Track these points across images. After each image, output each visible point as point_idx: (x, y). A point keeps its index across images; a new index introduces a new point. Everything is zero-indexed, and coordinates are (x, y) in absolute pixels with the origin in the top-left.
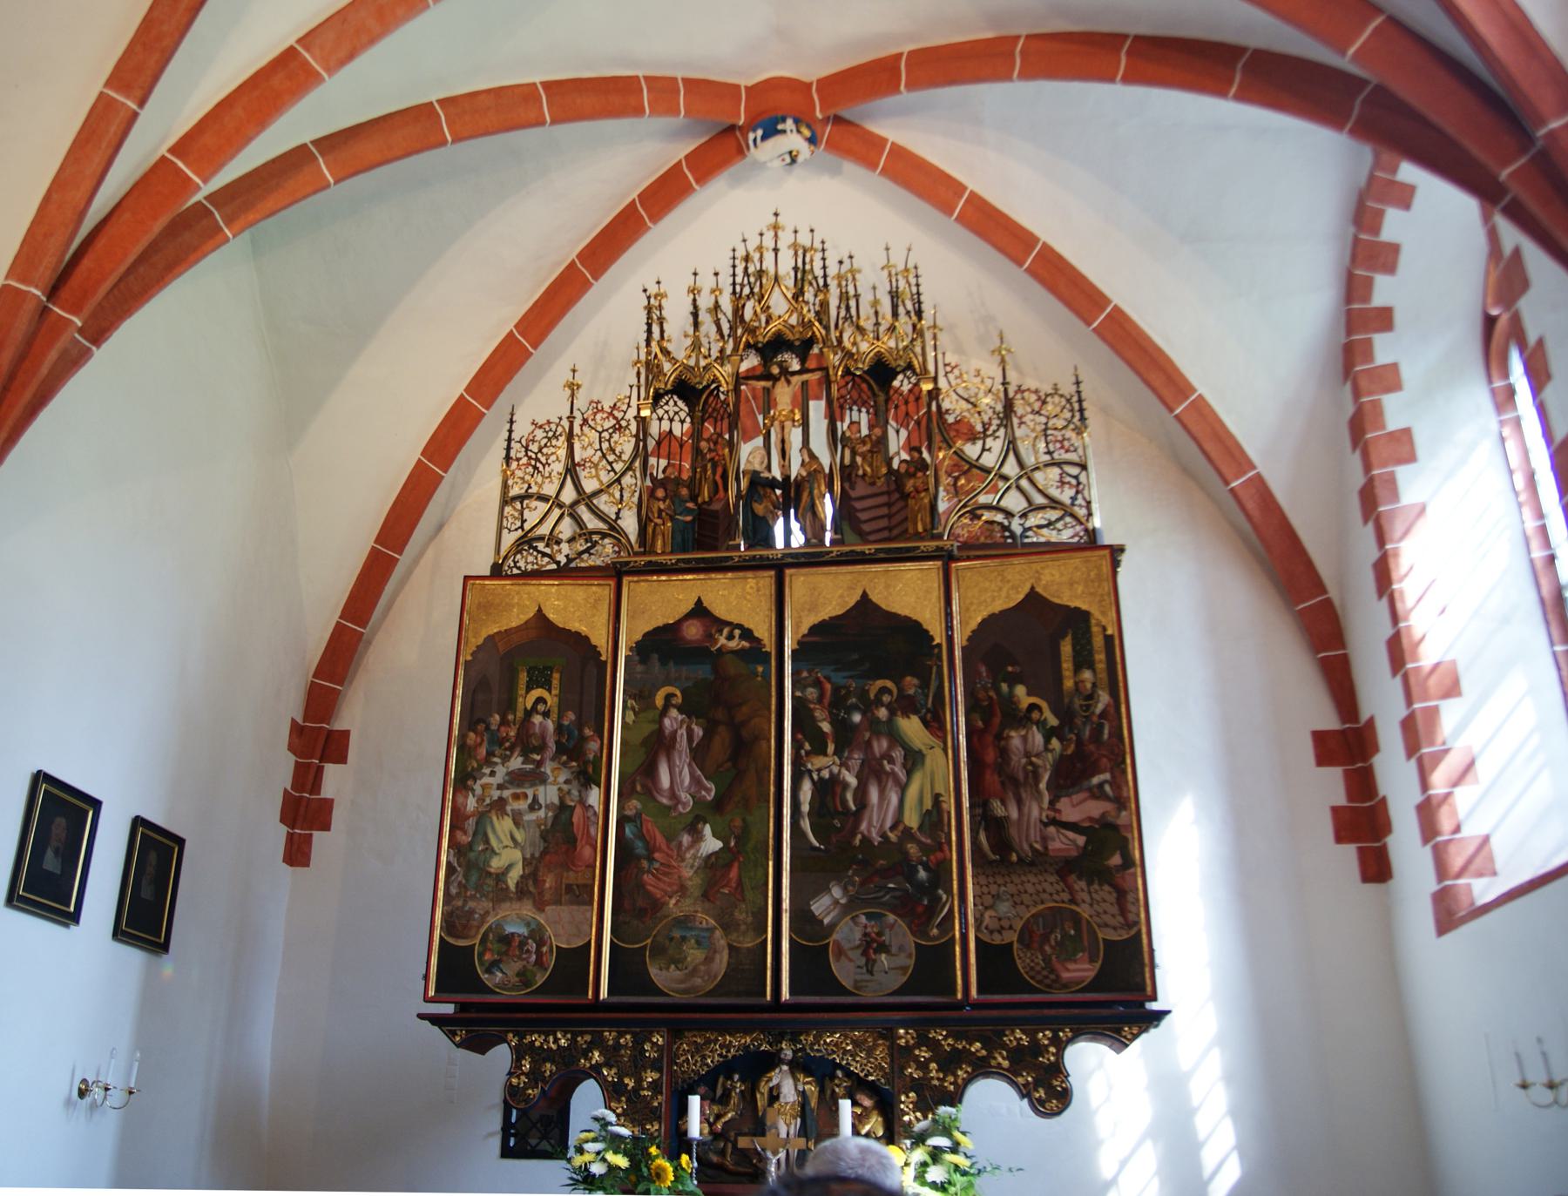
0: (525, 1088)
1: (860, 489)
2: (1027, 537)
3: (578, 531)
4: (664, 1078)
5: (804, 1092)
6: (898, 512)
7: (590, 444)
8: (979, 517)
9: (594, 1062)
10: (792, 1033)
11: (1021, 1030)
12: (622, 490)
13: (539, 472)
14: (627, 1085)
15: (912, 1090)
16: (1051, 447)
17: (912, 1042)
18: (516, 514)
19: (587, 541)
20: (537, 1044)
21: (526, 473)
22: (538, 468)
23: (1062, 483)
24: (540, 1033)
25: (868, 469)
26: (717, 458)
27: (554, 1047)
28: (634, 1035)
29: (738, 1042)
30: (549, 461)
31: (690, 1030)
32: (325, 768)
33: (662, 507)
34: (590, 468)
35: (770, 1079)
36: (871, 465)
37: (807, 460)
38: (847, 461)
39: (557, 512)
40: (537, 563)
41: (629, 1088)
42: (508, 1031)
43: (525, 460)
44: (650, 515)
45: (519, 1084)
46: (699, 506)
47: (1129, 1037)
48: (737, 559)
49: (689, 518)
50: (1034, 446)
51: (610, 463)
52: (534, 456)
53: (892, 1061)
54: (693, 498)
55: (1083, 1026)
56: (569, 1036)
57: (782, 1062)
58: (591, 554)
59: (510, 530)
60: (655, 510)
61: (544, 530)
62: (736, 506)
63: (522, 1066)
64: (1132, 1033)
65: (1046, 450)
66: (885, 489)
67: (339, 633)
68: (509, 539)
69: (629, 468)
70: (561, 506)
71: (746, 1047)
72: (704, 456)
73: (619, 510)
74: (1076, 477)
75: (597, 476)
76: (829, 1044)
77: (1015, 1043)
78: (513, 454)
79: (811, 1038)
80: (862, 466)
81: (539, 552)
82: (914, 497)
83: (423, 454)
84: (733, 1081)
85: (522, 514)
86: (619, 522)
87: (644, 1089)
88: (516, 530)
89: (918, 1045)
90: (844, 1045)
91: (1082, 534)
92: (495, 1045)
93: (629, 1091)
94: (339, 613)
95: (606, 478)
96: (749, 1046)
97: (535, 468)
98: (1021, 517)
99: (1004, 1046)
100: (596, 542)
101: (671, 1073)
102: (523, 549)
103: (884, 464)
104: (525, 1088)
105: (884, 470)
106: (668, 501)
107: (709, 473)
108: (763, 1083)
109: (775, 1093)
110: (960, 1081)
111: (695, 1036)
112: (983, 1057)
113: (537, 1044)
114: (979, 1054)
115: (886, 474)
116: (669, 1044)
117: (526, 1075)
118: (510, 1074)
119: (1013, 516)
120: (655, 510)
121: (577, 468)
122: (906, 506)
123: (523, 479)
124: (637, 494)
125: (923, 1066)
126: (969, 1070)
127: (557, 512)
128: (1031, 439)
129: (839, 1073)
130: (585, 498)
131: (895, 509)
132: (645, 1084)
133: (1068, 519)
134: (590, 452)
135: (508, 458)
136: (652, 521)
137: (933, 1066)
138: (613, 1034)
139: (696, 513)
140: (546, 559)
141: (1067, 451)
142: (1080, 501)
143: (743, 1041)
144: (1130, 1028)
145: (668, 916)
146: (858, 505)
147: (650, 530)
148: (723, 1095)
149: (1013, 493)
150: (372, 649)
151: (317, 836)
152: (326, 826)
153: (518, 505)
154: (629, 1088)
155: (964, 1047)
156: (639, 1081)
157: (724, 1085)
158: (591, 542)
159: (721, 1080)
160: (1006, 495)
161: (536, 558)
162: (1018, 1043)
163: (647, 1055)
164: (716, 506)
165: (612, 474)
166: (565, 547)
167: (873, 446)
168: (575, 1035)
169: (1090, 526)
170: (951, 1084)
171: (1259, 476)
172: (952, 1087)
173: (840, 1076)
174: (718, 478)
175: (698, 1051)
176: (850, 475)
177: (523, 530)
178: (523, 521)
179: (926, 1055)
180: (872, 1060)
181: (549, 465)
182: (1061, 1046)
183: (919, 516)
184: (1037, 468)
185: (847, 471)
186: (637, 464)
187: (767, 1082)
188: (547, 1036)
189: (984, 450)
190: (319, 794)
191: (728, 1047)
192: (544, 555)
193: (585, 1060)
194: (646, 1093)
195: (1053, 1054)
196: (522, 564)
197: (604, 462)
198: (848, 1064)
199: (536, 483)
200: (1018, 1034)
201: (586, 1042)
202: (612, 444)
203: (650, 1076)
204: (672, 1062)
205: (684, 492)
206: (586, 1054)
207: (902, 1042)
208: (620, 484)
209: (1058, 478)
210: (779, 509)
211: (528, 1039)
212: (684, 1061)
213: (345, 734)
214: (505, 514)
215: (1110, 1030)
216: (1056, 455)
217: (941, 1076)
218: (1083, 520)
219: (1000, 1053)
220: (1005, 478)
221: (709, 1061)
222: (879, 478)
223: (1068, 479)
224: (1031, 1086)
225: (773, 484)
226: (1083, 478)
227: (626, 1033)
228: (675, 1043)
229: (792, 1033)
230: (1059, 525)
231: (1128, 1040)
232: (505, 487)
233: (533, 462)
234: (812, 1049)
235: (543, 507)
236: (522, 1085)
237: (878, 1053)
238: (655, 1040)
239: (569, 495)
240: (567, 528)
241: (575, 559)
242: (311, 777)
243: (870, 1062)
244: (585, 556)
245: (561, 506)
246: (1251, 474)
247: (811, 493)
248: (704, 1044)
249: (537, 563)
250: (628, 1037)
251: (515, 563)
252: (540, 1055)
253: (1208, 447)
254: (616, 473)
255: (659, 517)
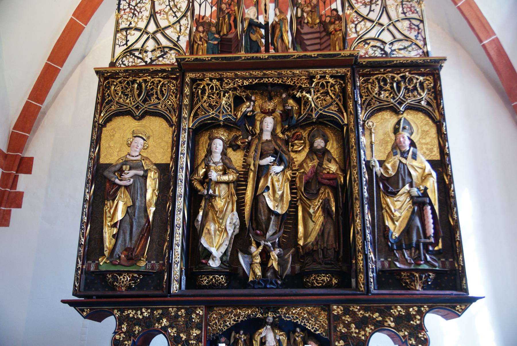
0: (124, 341)
1: (306, 29)
2: (393, 54)
3: (157, 46)
4: (203, 333)
5: (279, 340)
6: (325, 42)
7: (164, 3)
8: (369, 44)
9: (163, 325)
10: (274, 308)
11: (400, 306)
12: (180, 26)
13: (136, 16)
14: (182, 337)
15: (341, 339)
16: (405, 10)
17: (340, 312)
18: (123, 37)
19: (161, 51)
20: (131, 315)
21: (129, 17)
22: (135, 14)
23: (410, 28)
24: (132, 309)
25: (310, 19)
26: (231, 12)
27: (141, 317)
28: (186, 309)
29: (244, 313)
30: (141, 11)
31: (217, 307)
32: (19, 177)
33: (202, 36)
34: (164, 14)
35: (261, 333)
36: (311, 18)
37: (278, 13)
38: (299, 15)
39: (145, 37)
40: (134, 62)
41: (183, 339)
42: (114, 309)
43: (128, 10)
44: (195, 39)
45: (120, 338)
46: (221, 37)
47: (460, 311)
48: (243, 58)
49: (216, 42)
50: (396, 9)
51: (174, 13)
52: (133, 8)
53: (329, 322)
54: (218, 33)
55: (435, 304)
56: (149, 311)
57: (267, 323)
58: (164, 58)
59: (120, 46)
60: (198, 37)
61: (138, 45)
62: (241, 36)
63: (122, 328)
64: (461, 309)
65: (402, 12)
66: (318, 30)
67: (27, 106)
68: (119, 50)
69: (184, 15)
70: (147, 33)
71: (249, 315)
72: (223, 12)
73: (179, 36)
74: (418, 26)
75: (167, 19)
76: (294, 314)
77: (397, 313)
78: (121, 7)
79: (284, 311)
80: (307, 18)
81: (135, 56)
82: (334, 34)
83: (73, 15)
84: (240, 334)
85: (127, 37)
86: (179, 42)
87: (191, 340)
88: (123, 45)
89: (344, 314)
90: (302, 314)
91: (421, 54)
92: (107, 317)
93: (183, 341)
94: (28, 97)
95: (173, 20)
96: (250, 315)
97: (134, 14)
98: (390, 44)
99: (391, 315)
100: (167, 52)
101: (207, 330)
102: (127, 55)
103: (318, 18)
104: (124, 341)
105: (318, 21)
106: (205, 33)
107: (227, 20)
108: (257, 336)
109: (263, 341)
110: (368, 334)
111: (220, 310)
112: (380, 321)
113: (131, 315)
114: (377, 319)
115: (318, 23)
116: (206, 314)
117: (125, 333)
118: (115, 333)
119: (386, 43)
120: (198, 37)
121: (157, 14)
122: (330, 38)
123: (127, 19)
124: (188, 29)
125: (347, 326)
126: (373, 328)
127: (145, 37)
128: (395, 6)
129: (298, 330)
130: (161, 30)
131: (323, 40)
132: (192, 337)
133: (414, 46)
134: (164, 6)
135: (119, 9)
136: (196, 43)
137: (353, 326)
138: (174, 309)
139: (219, 40)
140: (140, 60)
141: (413, 13)
142: (420, 37)
143: (247, 312)
144: (461, 306)
145: (275, 148)
146: (305, 37)
147: (195, 47)
148: (234, 342)
149: (386, 32)
150: (46, 116)
151: (14, 211)
152: (19, 206)
153: (124, 33)
154: (183, 339)
155: (370, 315)
156: (189, 335)
157: (235, 337)
158: (164, 52)
159: (233, 334)
160: (382, 33)
161: (134, 60)
162: (399, 313)
163: (194, 320)
164: (230, 36)
165: (175, 18)
166: (150, 54)
167: (312, 8)
168: (153, 310)
169: (425, 50)
170: (363, 335)
171: (497, 39)
172: (363, 338)
173: (299, 331)
174: (231, 22)
175: (221, 317)
176: (301, 22)
177: (127, 45)
178: (127, 41)
179: (349, 320)
180: (318, 322)
181: (141, 12)
182: (423, 315)
183: (337, 43)
184: (398, 20)
185: (299, 20)
186: (189, 14)
187: (259, 334)
188: (137, 311)
189: (370, 11)
190: (16, 189)
191: (238, 315)
192: (138, 58)
193: (158, 324)
194: (192, 342)
195: (419, 320)
196: (126, 63)
197: (171, 12)
198: (305, 324)
199: (134, 21)
200: (399, 308)
201: (159, 314)
202: (176, 3)
203: (195, 332)
204: (207, 324)
205: (213, 29)
206: (159, 320)
207: (335, 313)
208: (179, 23)
209: (408, 26)
210: (263, 38)
211: (126, 312)
212: (214, 324)
213: (31, 159)
214: (117, 37)
215: (449, 306)
216: (407, 14)
217: (357, 331)
218: (422, 47)
219: (389, 319)
220: (382, 25)
221: (228, 323)
222: (315, 25)
223: (413, 27)
224: (407, 337)
225: (260, 26)
226: (421, 26)
227: (182, 308)
228: (209, 314)
229: (274, 308)
230: (410, 49)
231: (460, 312)
232: (117, 23)
233: (133, 11)
234: (285, 316)
235: (138, 34)
236: (121, 339)
237: (321, 318)
238: (198, 312)
239: (152, 28)
240: (151, 45)
241: (155, 60)
242: (11, 181)
243: (317, 323)
244: (161, 59)
245: (147, 33)
246: (493, 37)
247: (281, 30)
248: (225, 314)
249: (134, 62)
250: (183, 311)
251: (123, 62)
252: (132, 321)
253: (473, 23)
254: (177, 18)
255: (200, 40)
